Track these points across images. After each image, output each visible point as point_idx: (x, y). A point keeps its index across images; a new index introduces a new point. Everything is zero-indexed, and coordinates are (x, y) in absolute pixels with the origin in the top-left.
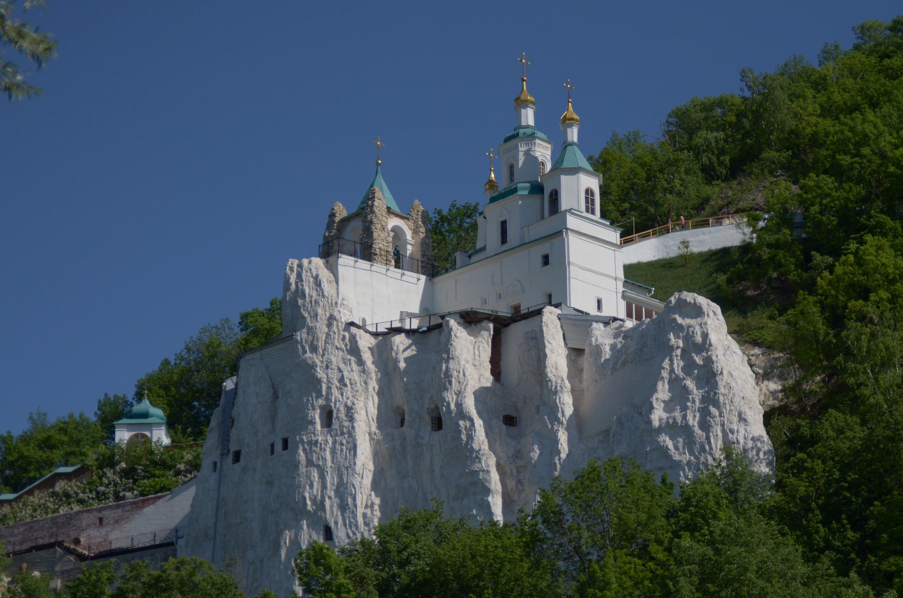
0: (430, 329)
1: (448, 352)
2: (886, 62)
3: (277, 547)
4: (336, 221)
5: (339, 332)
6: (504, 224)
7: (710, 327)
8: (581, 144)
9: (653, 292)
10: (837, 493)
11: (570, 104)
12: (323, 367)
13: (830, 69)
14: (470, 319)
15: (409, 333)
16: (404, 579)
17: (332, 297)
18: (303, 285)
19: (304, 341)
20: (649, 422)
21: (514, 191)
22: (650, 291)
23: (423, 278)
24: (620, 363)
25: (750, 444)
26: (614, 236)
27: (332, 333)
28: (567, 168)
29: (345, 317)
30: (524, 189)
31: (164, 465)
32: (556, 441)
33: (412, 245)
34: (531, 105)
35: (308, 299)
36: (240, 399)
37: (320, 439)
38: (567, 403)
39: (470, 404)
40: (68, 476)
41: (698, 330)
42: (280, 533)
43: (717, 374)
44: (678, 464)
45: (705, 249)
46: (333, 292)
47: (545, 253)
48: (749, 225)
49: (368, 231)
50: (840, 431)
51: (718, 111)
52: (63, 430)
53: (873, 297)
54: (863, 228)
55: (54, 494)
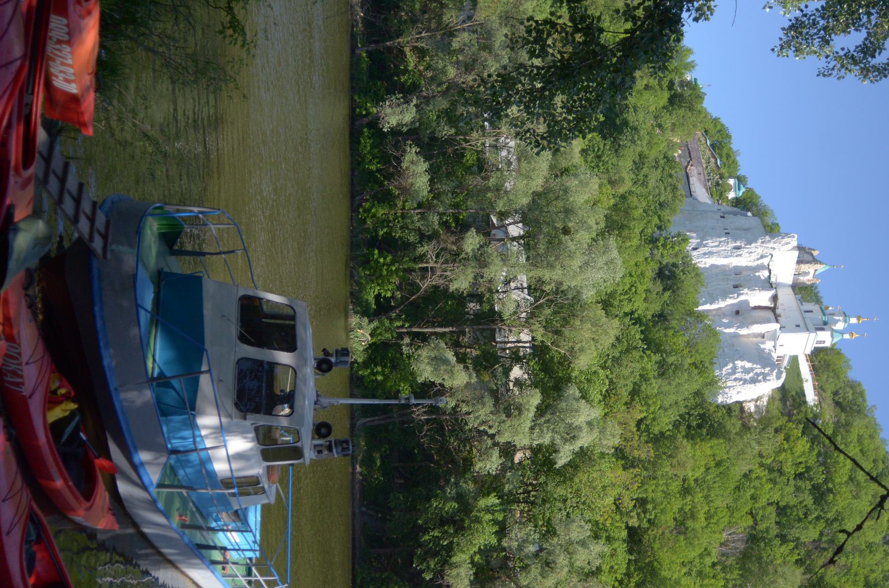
0: (771, 284)
1: (762, 290)
2: (881, 462)
3: (690, 231)
6: (812, 311)
8: (842, 340)
10: (710, 420)
13: (878, 441)
14: (775, 298)
15: (769, 277)
16: (677, 272)
20: (737, 360)
21: (824, 314)
23: (791, 283)
25: (729, 395)
26: (808, 352)
29: (774, 253)
31: (721, 195)
32: (730, 327)
36: (743, 217)
37: (729, 245)
38: (743, 332)
39: (742, 298)
40: (716, 163)
41: (771, 378)
42: (695, 232)
44: (721, 370)
45: (805, 388)
48: (815, 404)
49: (808, 262)
50: (734, 425)
51: (861, 399)
52: (733, 162)
53: (785, 442)
54: (813, 443)
55: (709, 158)
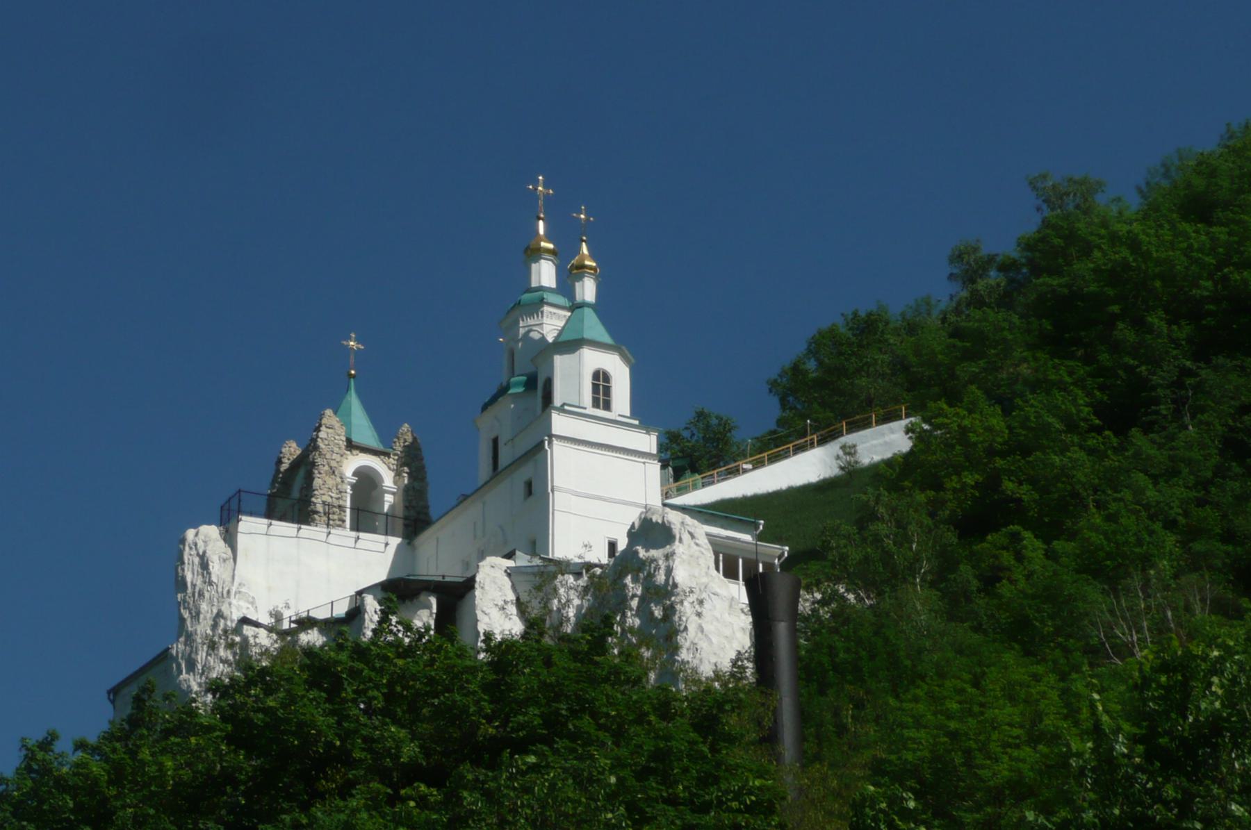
6: (495, 441)
7: (680, 557)
9: (761, 527)
11: (584, 244)
17: (224, 583)
18: (183, 570)
19: (180, 655)
22: (757, 527)
24: (197, 595)
28: (569, 341)
30: (517, 384)
33: (393, 494)
35: (190, 590)
43: (679, 631)
46: (226, 576)
47: (526, 478)
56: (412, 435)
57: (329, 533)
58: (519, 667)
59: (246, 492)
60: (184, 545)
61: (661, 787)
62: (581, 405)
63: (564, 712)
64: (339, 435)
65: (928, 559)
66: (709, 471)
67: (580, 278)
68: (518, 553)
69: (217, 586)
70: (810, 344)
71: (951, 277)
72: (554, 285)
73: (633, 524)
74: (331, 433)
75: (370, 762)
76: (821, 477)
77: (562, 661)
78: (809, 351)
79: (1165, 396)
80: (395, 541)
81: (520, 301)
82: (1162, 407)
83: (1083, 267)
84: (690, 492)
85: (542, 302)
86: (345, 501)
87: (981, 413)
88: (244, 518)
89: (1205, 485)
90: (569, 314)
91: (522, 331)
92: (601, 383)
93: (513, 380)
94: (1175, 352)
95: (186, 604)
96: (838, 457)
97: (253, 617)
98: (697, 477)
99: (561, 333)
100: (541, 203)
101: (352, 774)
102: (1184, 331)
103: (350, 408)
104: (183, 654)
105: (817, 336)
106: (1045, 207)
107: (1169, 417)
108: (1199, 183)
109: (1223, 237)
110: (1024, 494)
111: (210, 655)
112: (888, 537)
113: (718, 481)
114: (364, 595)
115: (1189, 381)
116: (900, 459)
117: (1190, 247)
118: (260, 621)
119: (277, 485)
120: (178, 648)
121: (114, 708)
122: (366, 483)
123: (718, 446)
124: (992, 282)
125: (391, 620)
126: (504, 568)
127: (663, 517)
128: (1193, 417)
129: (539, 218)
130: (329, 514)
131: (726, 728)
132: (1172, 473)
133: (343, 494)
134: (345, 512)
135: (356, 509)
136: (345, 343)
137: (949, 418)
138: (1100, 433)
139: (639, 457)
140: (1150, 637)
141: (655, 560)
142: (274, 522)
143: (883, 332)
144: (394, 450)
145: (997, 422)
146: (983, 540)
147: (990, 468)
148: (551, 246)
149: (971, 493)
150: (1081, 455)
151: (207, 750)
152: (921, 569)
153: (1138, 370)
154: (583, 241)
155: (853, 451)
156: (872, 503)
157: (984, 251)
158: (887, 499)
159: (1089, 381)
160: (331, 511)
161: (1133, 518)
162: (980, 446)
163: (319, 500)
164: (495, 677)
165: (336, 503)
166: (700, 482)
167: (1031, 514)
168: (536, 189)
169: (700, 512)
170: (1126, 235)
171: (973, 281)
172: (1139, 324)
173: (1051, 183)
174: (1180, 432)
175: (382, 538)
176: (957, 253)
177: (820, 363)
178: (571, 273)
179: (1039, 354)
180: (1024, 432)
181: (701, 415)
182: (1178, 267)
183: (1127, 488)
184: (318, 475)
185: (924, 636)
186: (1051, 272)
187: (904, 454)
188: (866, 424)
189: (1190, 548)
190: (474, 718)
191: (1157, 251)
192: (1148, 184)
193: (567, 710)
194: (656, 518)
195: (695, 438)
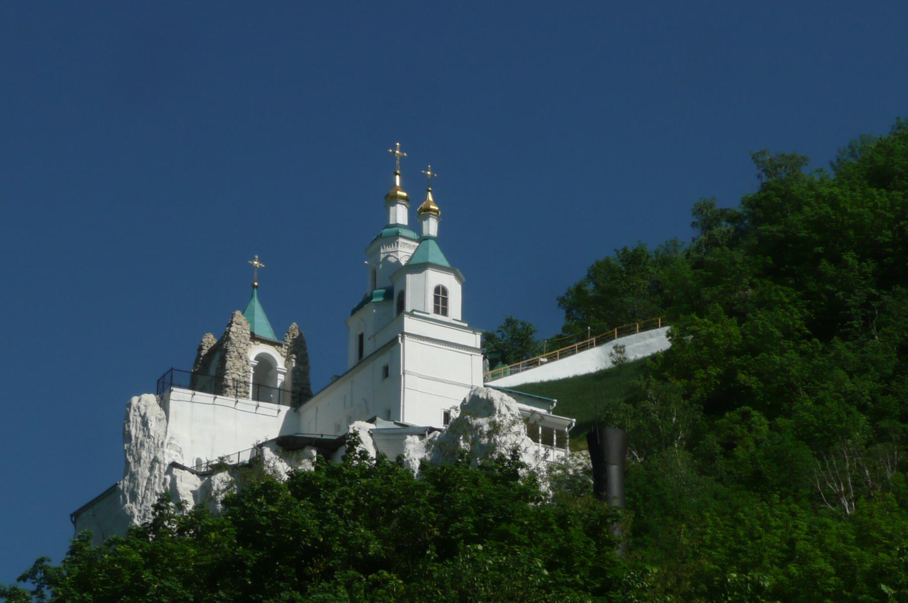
4: (202, 354)
5: (160, 476)
6: (361, 337)
9: (555, 404)
12: (140, 517)
17: (159, 436)
18: (129, 426)
19: (125, 489)
22: (552, 404)
24: (139, 445)
27: (152, 478)
29: (167, 459)
33: (284, 374)
34: (401, 201)
35: (133, 442)
46: (161, 431)
56: (299, 331)
57: (237, 402)
58: (456, 487)
59: (176, 370)
60: (130, 408)
61: (565, 575)
62: (426, 311)
63: (491, 520)
64: (246, 330)
65: (684, 430)
66: (515, 363)
67: (426, 218)
68: (378, 419)
69: (154, 439)
70: (590, 272)
71: (694, 224)
72: (406, 223)
73: (465, 399)
74: (239, 328)
75: (346, 554)
76: (599, 369)
77: (486, 485)
78: (589, 277)
79: (856, 314)
80: (285, 409)
81: (381, 234)
82: (855, 322)
83: (795, 218)
84: (501, 378)
85: (397, 235)
86: (249, 378)
87: (722, 323)
88: (175, 389)
89: (887, 379)
90: (417, 244)
91: (382, 256)
92: (441, 295)
93: (375, 292)
94: (864, 282)
95: (131, 452)
96: (611, 355)
97: (180, 461)
98: (507, 367)
99: (410, 259)
100: (398, 162)
101: (332, 563)
102: (870, 267)
103: (254, 311)
104: (127, 488)
105: (595, 265)
106: (763, 175)
107: (860, 329)
108: (880, 160)
109: (900, 199)
110: (753, 383)
111: (148, 489)
112: (654, 412)
113: (522, 370)
114: (264, 447)
115: (874, 304)
116: (662, 356)
117: (875, 206)
118: (185, 465)
119: (198, 366)
120: (124, 484)
121: (75, 527)
122: (265, 365)
123: (522, 345)
124: (724, 229)
125: (355, 450)
126: (368, 430)
127: (487, 395)
128: (878, 329)
129: (396, 174)
130: (237, 388)
131: (607, 536)
132: (862, 371)
133: (247, 373)
134: (249, 386)
135: (258, 385)
136: (251, 262)
137: (699, 327)
138: (810, 340)
139: (467, 351)
140: (853, 489)
141: (481, 426)
142: (197, 393)
143: (645, 264)
144: (286, 341)
145: (735, 330)
146: (722, 416)
147: (728, 364)
148: (405, 194)
149: (714, 382)
150: (795, 356)
151: (224, 542)
152: (678, 436)
153: (836, 295)
154: (429, 191)
155: (622, 350)
156: (644, 388)
157: (718, 206)
158: (654, 384)
159: (800, 303)
160: (239, 385)
161: (835, 403)
162: (721, 347)
163: (230, 377)
164: (439, 494)
165: (242, 379)
166: (509, 371)
167: (758, 398)
168: (394, 152)
169: (510, 392)
170: (829, 195)
171: (710, 228)
172: (837, 260)
173: (769, 158)
174: (868, 340)
175: (275, 406)
176: (698, 207)
177: (597, 285)
178: (420, 214)
179: (766, 281)
180: (753, 338)
181: (510, 322)
182: (867, 220)
183: (830, 380)
184: (230, 359)
185: (683, 485)
186: (772, 222)
187: (664, 352)
188: (630, 331)
189: (877, 425)
190: (424, 523)
191: (851, 208)
192: (838, 160)
193: (493, 518)
194: (482, 395)
195: (505, 338)
